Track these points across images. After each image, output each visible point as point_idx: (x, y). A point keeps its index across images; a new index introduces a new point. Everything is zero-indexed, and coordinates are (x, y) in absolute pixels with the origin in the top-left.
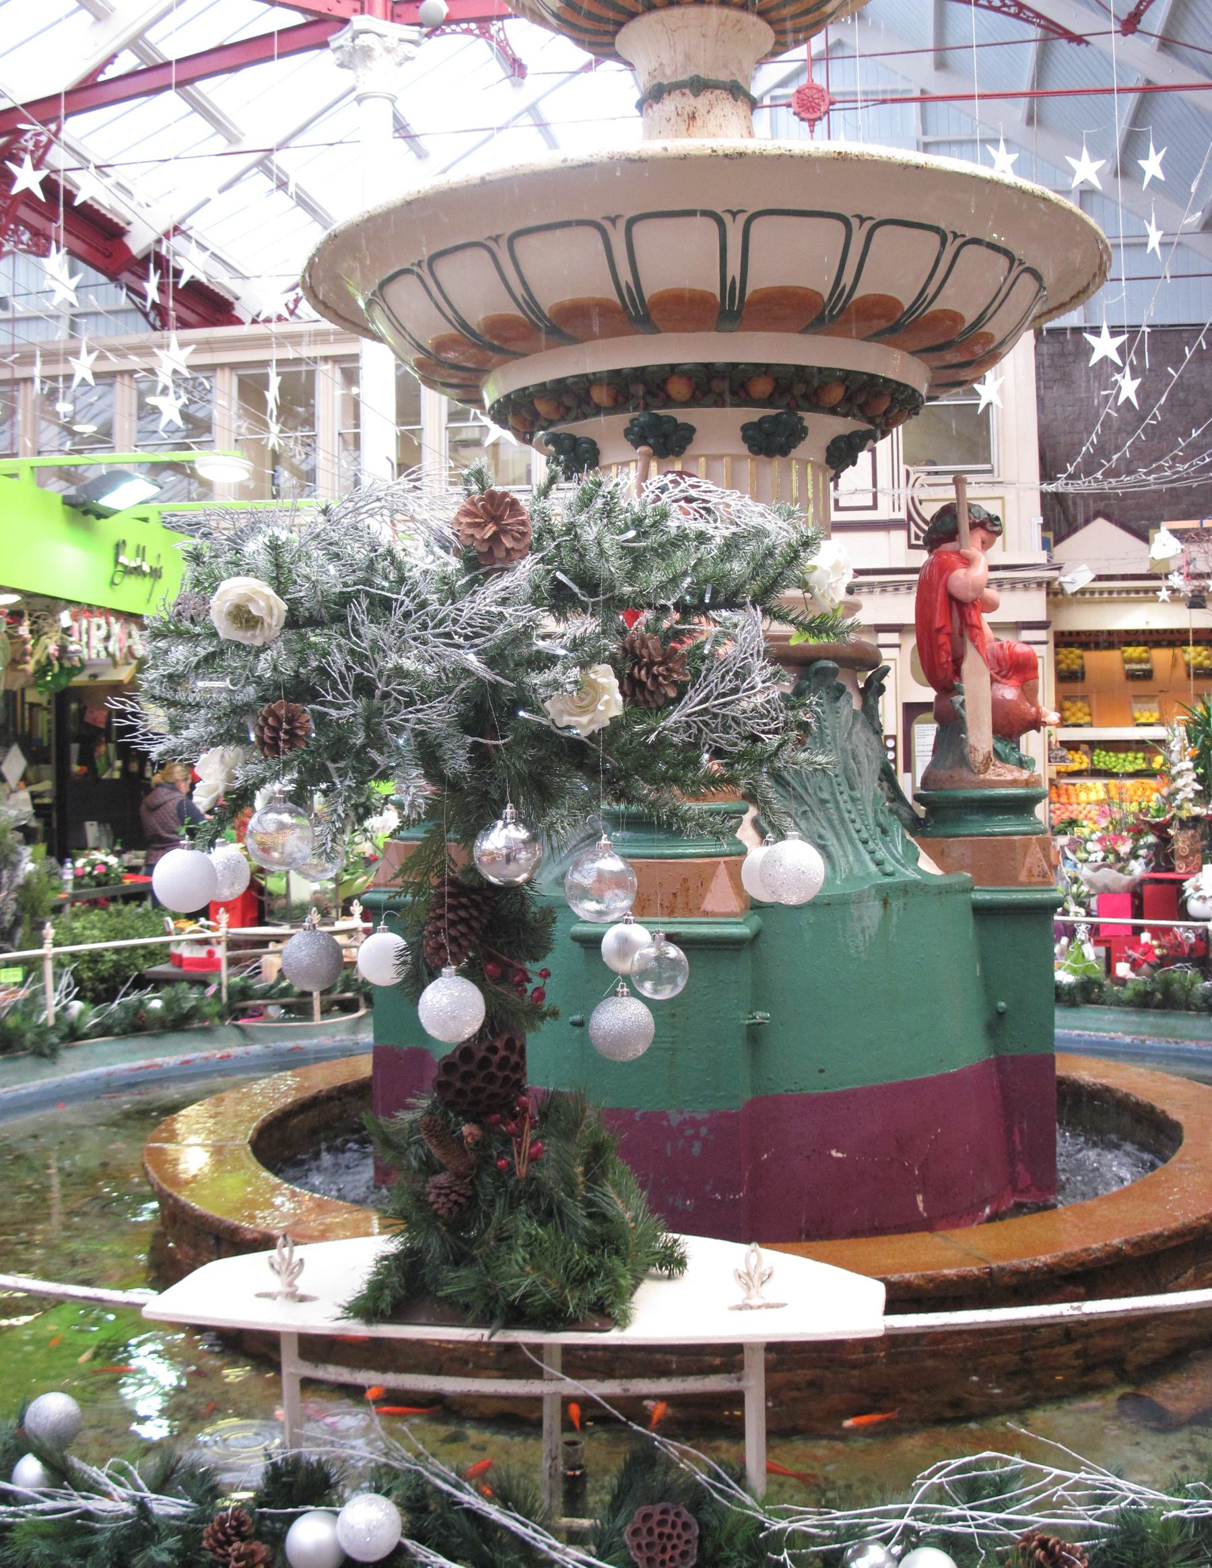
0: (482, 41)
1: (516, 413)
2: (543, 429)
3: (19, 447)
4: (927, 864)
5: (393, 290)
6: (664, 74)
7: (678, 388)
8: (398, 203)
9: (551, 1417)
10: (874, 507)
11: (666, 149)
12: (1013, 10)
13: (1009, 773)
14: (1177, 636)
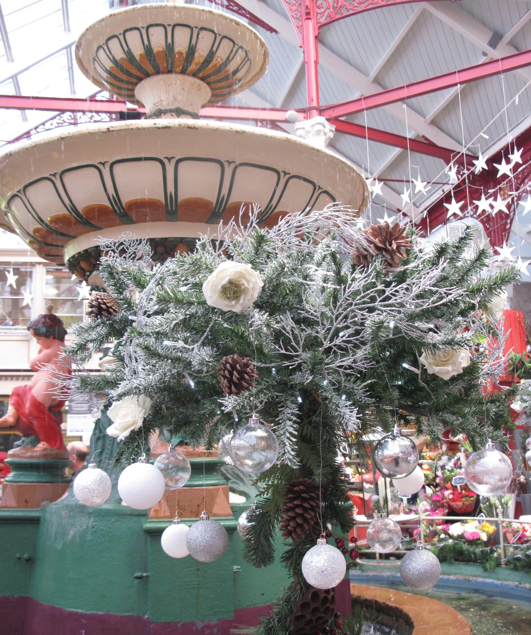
6: (162, 105)
8: (55, 138)
11: (208, 125)
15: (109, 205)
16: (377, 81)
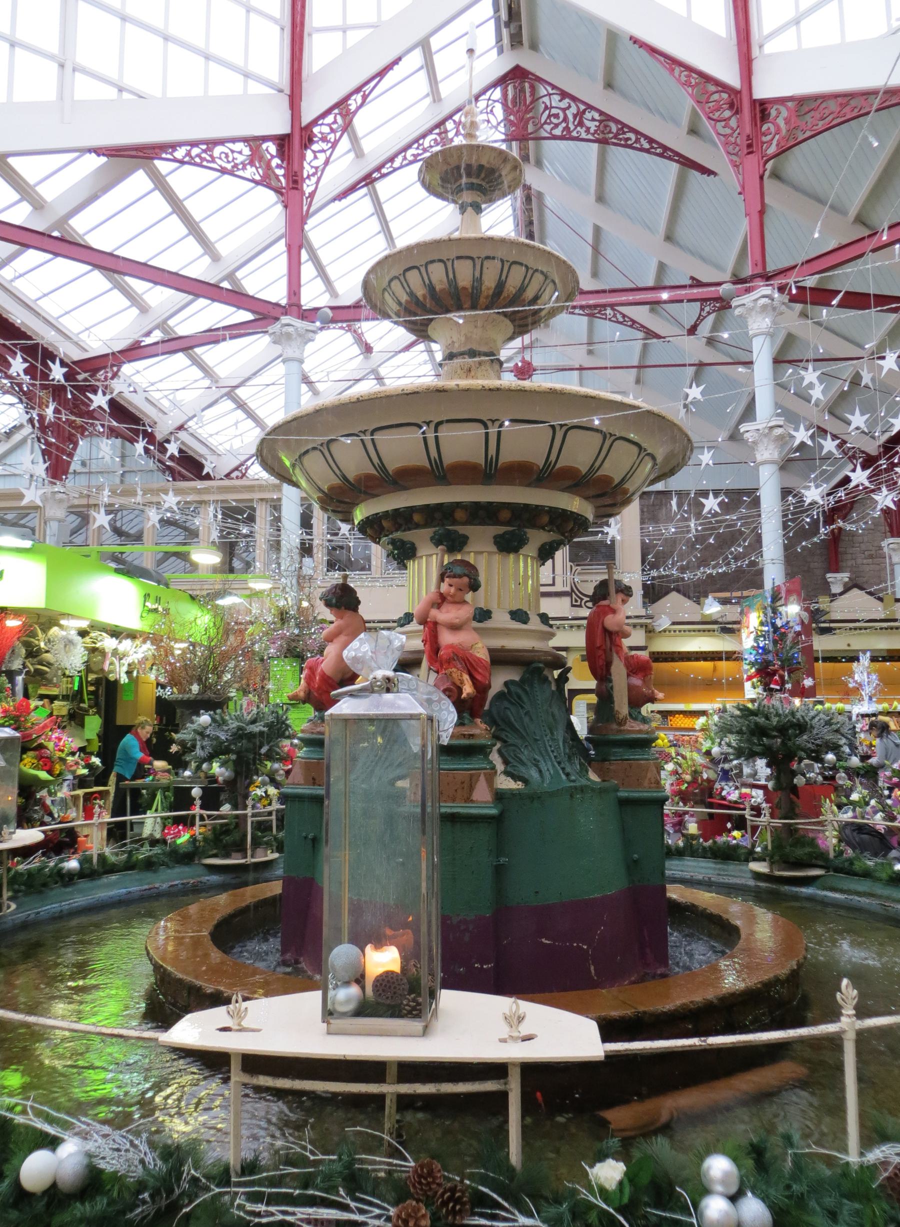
0: (349, 334)
1: (372, 527)
2: (386, 536)
3: (90, 542)
4: (593, 776)
5: (306, 460)
7: (459, 515)
9: (390, 1105)
10: (553, 584)
12: (629, 323)
13: (637, 726)
14: (716, 655)
15: (375, 472)
16: (860, 220)
